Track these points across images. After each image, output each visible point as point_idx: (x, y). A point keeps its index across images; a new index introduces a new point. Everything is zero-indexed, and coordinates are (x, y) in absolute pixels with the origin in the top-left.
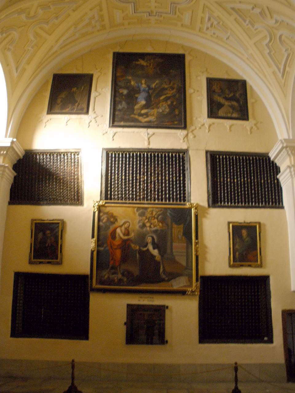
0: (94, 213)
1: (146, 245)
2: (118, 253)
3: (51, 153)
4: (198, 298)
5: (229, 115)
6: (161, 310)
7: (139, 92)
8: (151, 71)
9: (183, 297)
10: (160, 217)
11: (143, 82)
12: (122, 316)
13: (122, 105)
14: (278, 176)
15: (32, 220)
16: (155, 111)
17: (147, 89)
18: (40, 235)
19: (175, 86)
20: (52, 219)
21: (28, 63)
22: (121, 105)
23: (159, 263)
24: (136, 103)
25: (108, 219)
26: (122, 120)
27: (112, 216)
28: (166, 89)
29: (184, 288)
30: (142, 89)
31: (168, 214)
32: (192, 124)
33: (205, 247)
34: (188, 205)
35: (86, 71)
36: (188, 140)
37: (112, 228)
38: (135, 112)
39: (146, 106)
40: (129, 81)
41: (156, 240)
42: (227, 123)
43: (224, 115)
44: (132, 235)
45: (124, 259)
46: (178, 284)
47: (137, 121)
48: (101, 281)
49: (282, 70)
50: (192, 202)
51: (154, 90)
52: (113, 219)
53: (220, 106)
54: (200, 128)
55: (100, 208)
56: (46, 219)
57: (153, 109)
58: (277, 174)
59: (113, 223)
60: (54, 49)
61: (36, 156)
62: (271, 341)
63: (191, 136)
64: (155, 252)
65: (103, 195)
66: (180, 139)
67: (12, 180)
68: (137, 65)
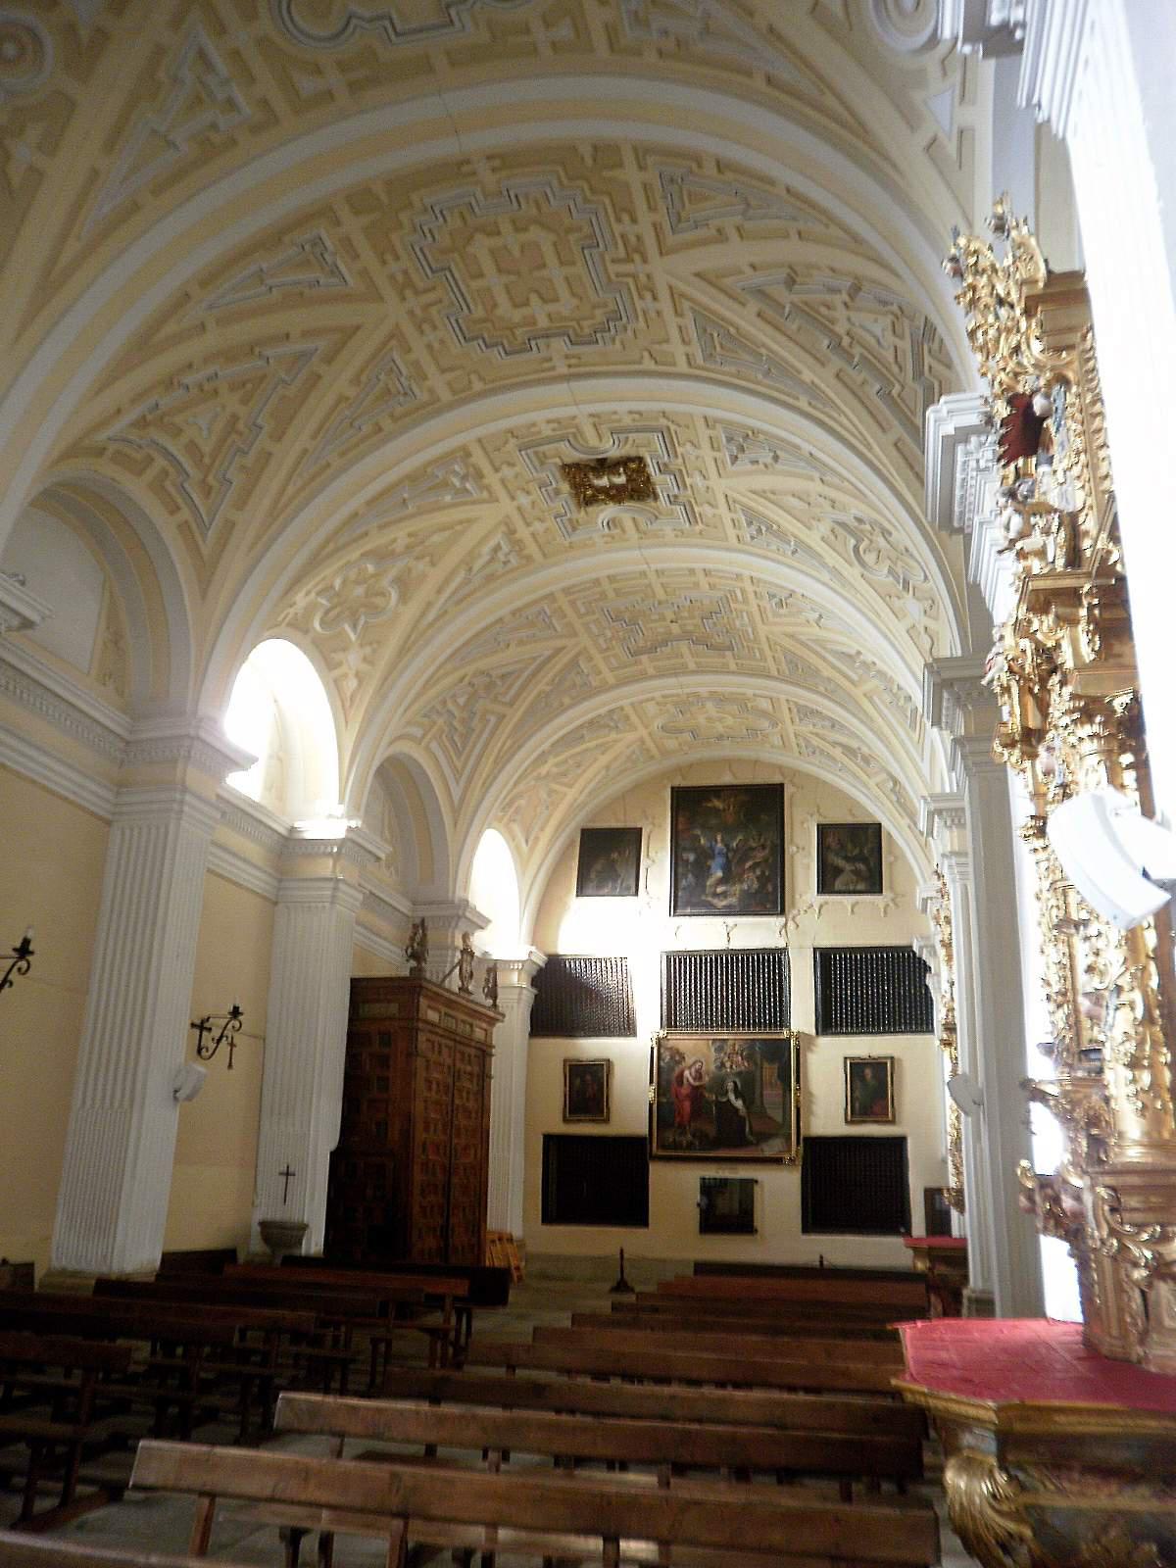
0: (652, 1048)
5: (851, 888)
6: (748, 1185)
7: (713, 857)
8: (730, 818)
11: (719, 838)
16: (737, 888)
18: (578, 1081)
21: (542, 829)
24: (709, 875)
25: (672, 1058)
27: (678, 1052)
28: (752, 849)
30: (716, 852)
32: (793, 905)
33: (811, 1094)
34: (785, 1034)
35: (630, 825)
37: (677, 1070)
39: (721, 882)
40: (697, 838)
42: (848, 900)
43: (844, 888)
46: (770, 1149)
47: (711, 905)
48: (662, 1146)
51: (735, 851)
52: (678, 1056)
53: (838, 871)
55: (659, 1041)
57: (734, 884)
59: (679, 1063)
60: (579, 801)
64: (739, 1104)
67: (532, 1001)
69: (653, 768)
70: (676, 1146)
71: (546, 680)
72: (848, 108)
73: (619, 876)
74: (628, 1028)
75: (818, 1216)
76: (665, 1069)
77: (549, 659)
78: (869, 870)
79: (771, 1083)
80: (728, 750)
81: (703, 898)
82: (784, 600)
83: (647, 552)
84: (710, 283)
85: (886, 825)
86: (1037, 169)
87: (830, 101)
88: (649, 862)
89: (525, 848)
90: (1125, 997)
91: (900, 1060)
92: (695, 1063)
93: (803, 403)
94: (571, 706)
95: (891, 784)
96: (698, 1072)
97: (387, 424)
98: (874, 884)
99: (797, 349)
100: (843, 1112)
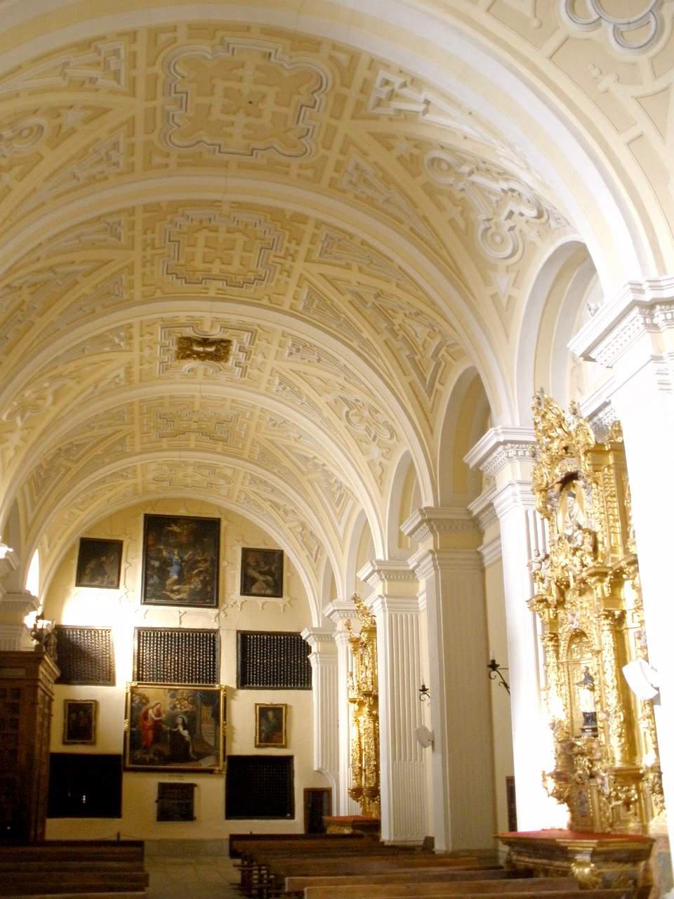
0: (127, 693)
1: (176, 726)
2: (150, 734)
3: (82, 630)
4: (225, 777)
5: (263, 592)
6: (191, 787)
7: (171, 565)
8: (184, 539)
9: (210, 775)
10: (191, 698)
11: (176, 553)
12: (153, 793)
13: (154, 580)
14: (308, 657)
15: (66, 701)
16: (186, 588)
17: (180, 561)
18: (74, 715)
19: (209, 558)
20: (85, 699)
21: (59, 538)
22: (153, 579)
23: (189, 742)
25: (140, 702)
26: (154, 596)
28: (199, 562)
29: (212, 768)
30: (174, 561)
31: (198, 696)
32: (224, 602)
33: (232, 728)
34: (217, 687)
36: (219, 620)
37: (144, 709)
38: (167, 587)
39: (178, 582)
40: (160, 551)
41: (186, 721)
42: (260, 600)
44: (164, 716)
45: (156, 739)
46: (206, 763)
47: (168, 598)
48: (133, 761)
49: (314, 557)
50: (221, 683)
51: (187, 562)
52: (145, 700)
53: (254, 581)
54: (232, 606)
55: (133, 690)
56: (78, 699)
57: (185, 585)
58: (308, 655)
59: (145, 704)
61: (66, 631)
62: (292, 817)
63: (222, 615)
64: (185, 733)
65: (136, 676)
66: (211, 618)
68: (170, 531)
69: (134, 501)
70: (143, 762)
71: (102, 449)
72: (454, 262)
73: (106, 573)
74: (109, 679)
75: (234, 809)
76: (136, 708)
77: (111, 435)
78: (275, 580)
79: (207, 719)
80: (188, 494)
81: (164, 592)
82: (279, 424)
83: (203, 387)
84: (328, 281)
85: (289, 553)
86: (540, 325)
87: (444, 253)
88: (128, 565)
89: (47, 550)
90: (618, 714)
91: (291, 707)
92: (157, 704)
93: (355, 344)
94: (108, 464)
95: (300, 529)
96: (158, 711)
97: (99, 309)
98: (277, 590)
99: (361, 317)
100: (254, 739)
